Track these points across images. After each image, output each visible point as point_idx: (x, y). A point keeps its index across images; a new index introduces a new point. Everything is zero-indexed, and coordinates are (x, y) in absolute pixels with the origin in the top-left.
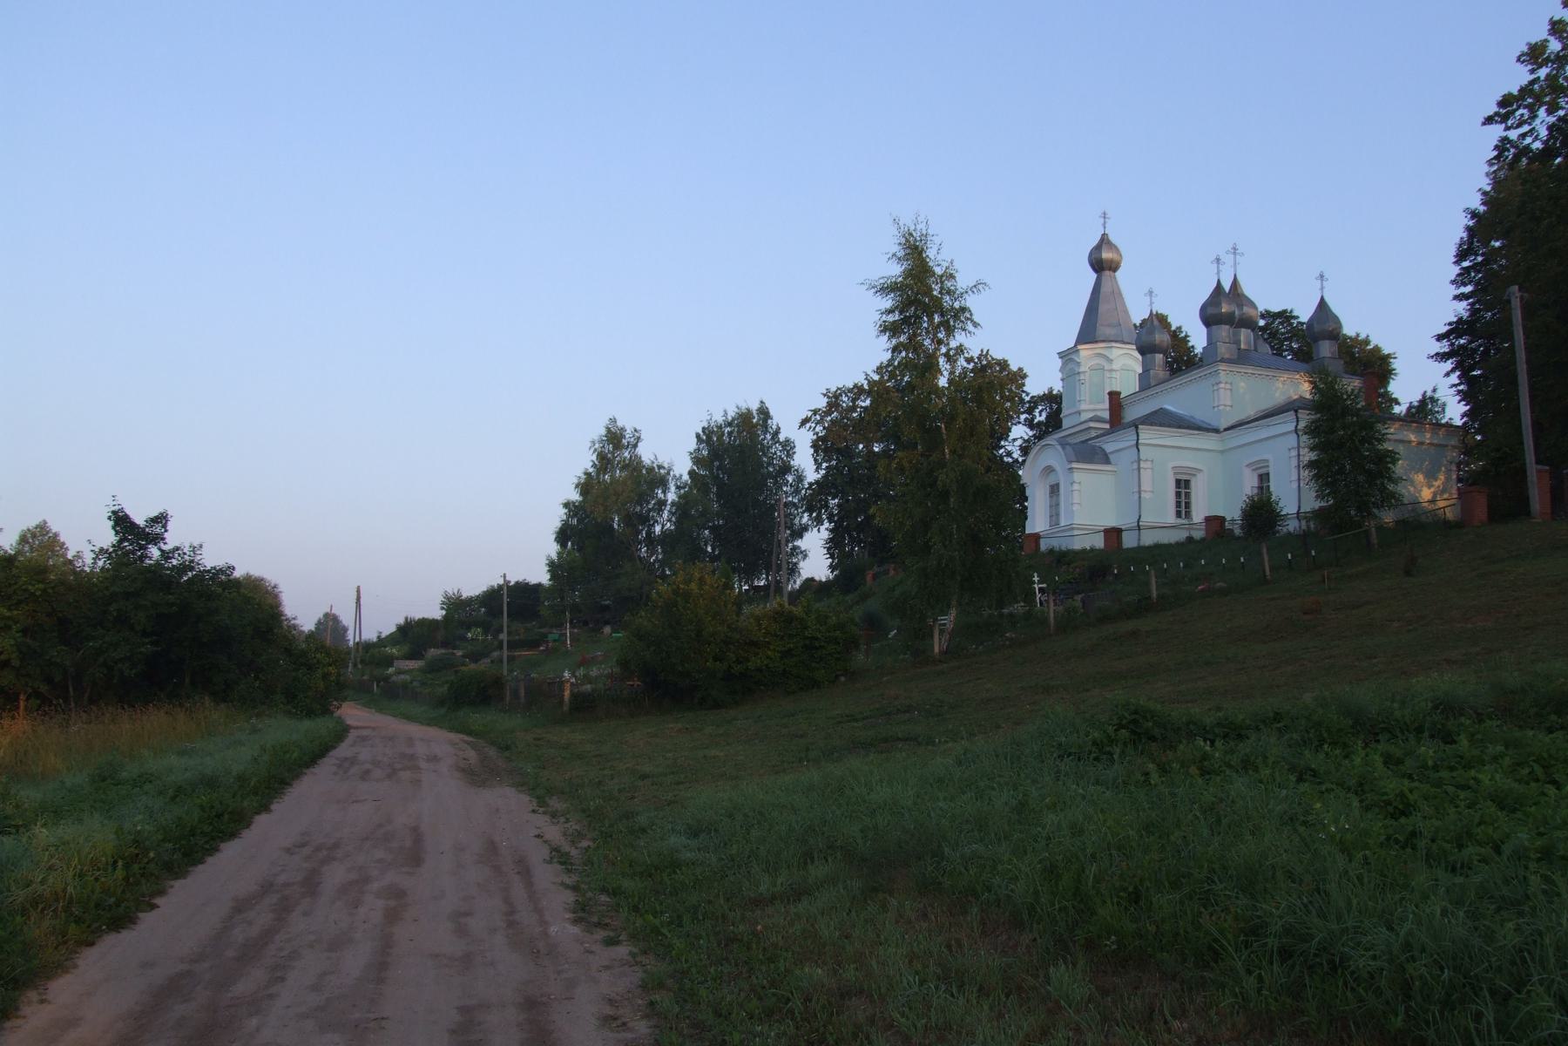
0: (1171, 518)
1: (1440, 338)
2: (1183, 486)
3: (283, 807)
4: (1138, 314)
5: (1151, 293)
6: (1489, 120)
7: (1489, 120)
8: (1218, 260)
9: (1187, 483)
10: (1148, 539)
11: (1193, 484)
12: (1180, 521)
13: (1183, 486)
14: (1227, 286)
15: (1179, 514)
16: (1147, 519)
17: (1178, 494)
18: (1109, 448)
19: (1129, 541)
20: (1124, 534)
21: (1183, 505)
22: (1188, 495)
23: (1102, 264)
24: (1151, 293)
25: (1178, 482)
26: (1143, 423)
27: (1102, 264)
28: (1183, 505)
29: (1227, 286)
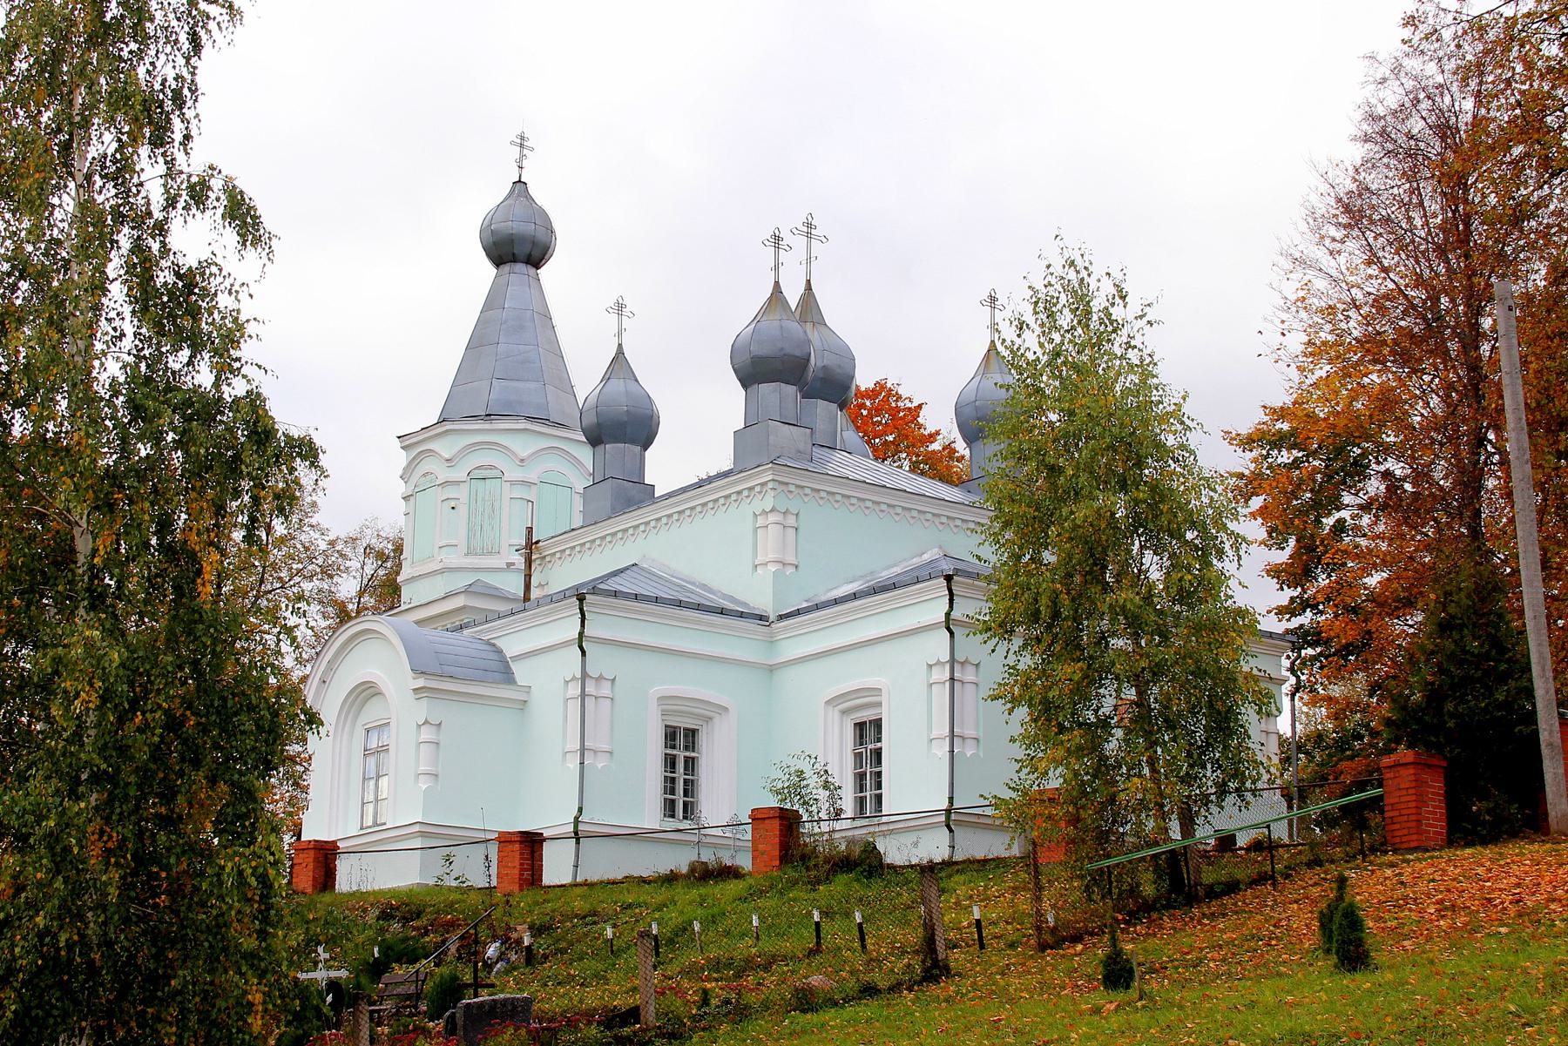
0: (650, 816)
1: (1248, 442)
2: (681, 742)
3: (664, 869)
4: (586, 377)
5: (620, 307)
6: (920, 406)
7: (920, 406)
8: (777, 239)
9: (691, 734)
10: (605, 864)
11: (703, 740)
12: (671, 824)
13: (681, 742)
14: (793, 296)
15: (670, 809)
16: (599, 816)
17: (670, 762)
18: (512, 645)
19: (557, 867)
20: (548, 849)
21: (680, 791)
22: (691, 764)
23: (518, 248)
24: (620, 307)
25: (671, 735)
26: (595, 591)
27: (518, 248)
28: (680, 791)
29: (793, 296)
